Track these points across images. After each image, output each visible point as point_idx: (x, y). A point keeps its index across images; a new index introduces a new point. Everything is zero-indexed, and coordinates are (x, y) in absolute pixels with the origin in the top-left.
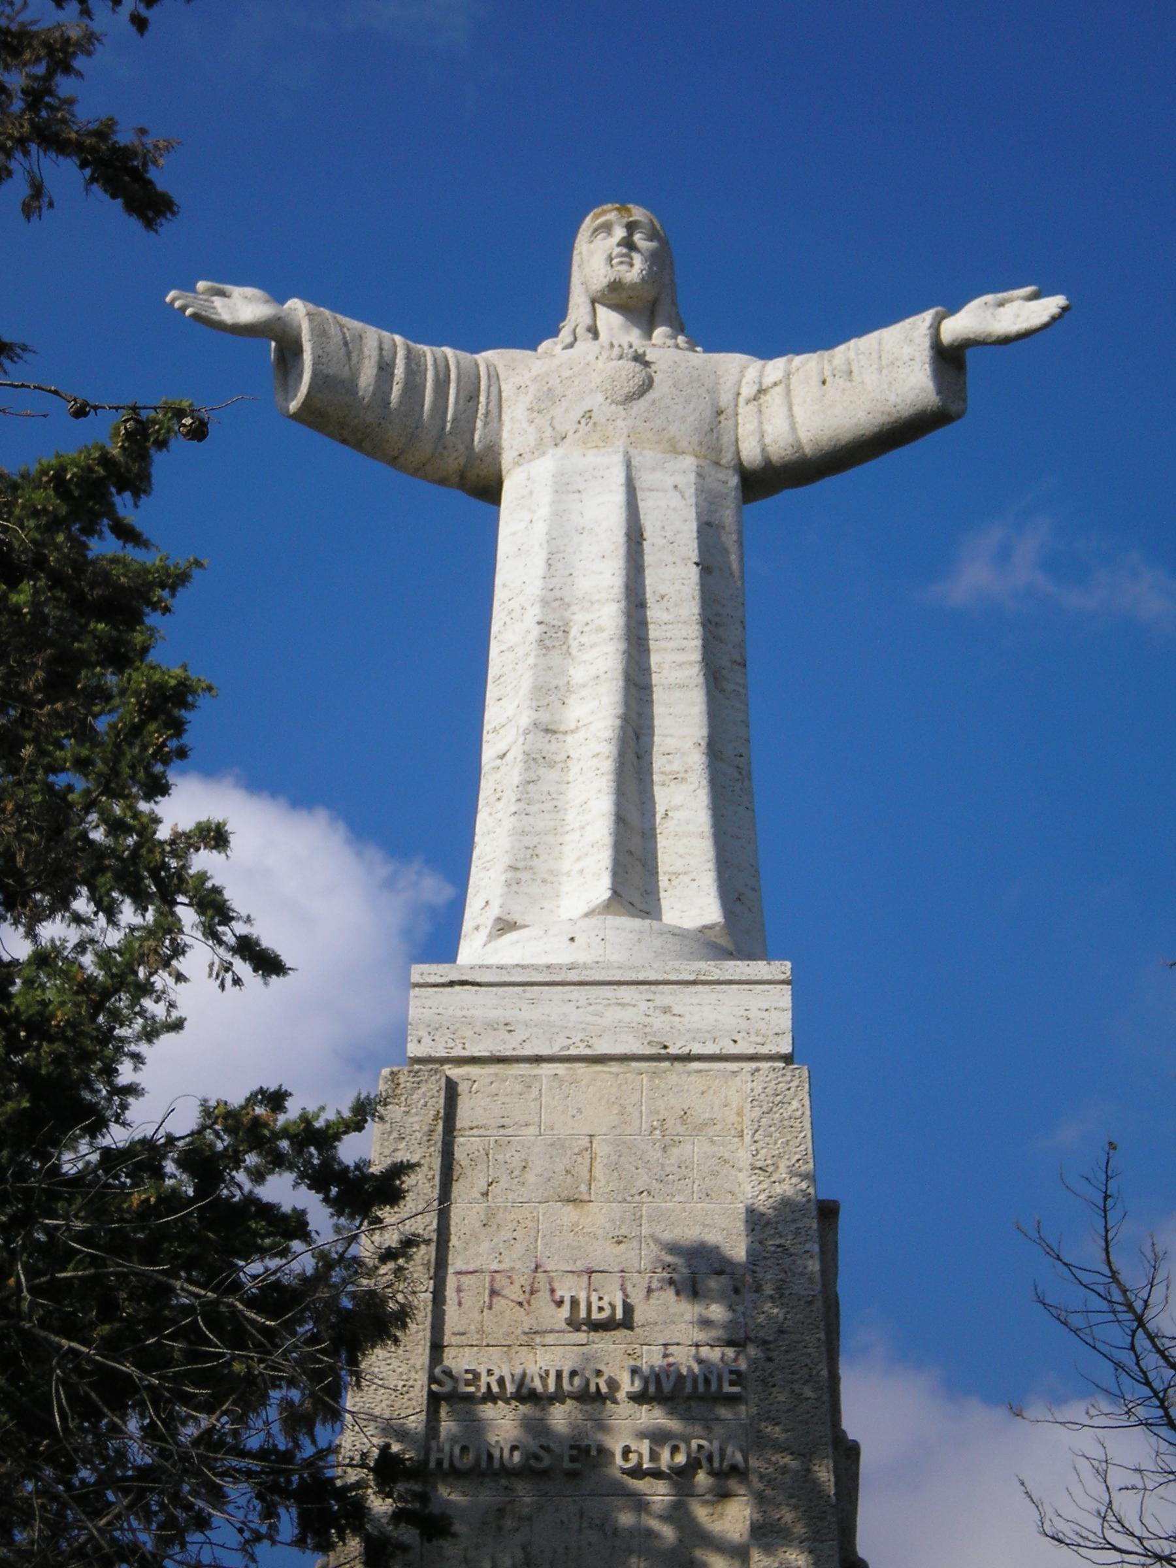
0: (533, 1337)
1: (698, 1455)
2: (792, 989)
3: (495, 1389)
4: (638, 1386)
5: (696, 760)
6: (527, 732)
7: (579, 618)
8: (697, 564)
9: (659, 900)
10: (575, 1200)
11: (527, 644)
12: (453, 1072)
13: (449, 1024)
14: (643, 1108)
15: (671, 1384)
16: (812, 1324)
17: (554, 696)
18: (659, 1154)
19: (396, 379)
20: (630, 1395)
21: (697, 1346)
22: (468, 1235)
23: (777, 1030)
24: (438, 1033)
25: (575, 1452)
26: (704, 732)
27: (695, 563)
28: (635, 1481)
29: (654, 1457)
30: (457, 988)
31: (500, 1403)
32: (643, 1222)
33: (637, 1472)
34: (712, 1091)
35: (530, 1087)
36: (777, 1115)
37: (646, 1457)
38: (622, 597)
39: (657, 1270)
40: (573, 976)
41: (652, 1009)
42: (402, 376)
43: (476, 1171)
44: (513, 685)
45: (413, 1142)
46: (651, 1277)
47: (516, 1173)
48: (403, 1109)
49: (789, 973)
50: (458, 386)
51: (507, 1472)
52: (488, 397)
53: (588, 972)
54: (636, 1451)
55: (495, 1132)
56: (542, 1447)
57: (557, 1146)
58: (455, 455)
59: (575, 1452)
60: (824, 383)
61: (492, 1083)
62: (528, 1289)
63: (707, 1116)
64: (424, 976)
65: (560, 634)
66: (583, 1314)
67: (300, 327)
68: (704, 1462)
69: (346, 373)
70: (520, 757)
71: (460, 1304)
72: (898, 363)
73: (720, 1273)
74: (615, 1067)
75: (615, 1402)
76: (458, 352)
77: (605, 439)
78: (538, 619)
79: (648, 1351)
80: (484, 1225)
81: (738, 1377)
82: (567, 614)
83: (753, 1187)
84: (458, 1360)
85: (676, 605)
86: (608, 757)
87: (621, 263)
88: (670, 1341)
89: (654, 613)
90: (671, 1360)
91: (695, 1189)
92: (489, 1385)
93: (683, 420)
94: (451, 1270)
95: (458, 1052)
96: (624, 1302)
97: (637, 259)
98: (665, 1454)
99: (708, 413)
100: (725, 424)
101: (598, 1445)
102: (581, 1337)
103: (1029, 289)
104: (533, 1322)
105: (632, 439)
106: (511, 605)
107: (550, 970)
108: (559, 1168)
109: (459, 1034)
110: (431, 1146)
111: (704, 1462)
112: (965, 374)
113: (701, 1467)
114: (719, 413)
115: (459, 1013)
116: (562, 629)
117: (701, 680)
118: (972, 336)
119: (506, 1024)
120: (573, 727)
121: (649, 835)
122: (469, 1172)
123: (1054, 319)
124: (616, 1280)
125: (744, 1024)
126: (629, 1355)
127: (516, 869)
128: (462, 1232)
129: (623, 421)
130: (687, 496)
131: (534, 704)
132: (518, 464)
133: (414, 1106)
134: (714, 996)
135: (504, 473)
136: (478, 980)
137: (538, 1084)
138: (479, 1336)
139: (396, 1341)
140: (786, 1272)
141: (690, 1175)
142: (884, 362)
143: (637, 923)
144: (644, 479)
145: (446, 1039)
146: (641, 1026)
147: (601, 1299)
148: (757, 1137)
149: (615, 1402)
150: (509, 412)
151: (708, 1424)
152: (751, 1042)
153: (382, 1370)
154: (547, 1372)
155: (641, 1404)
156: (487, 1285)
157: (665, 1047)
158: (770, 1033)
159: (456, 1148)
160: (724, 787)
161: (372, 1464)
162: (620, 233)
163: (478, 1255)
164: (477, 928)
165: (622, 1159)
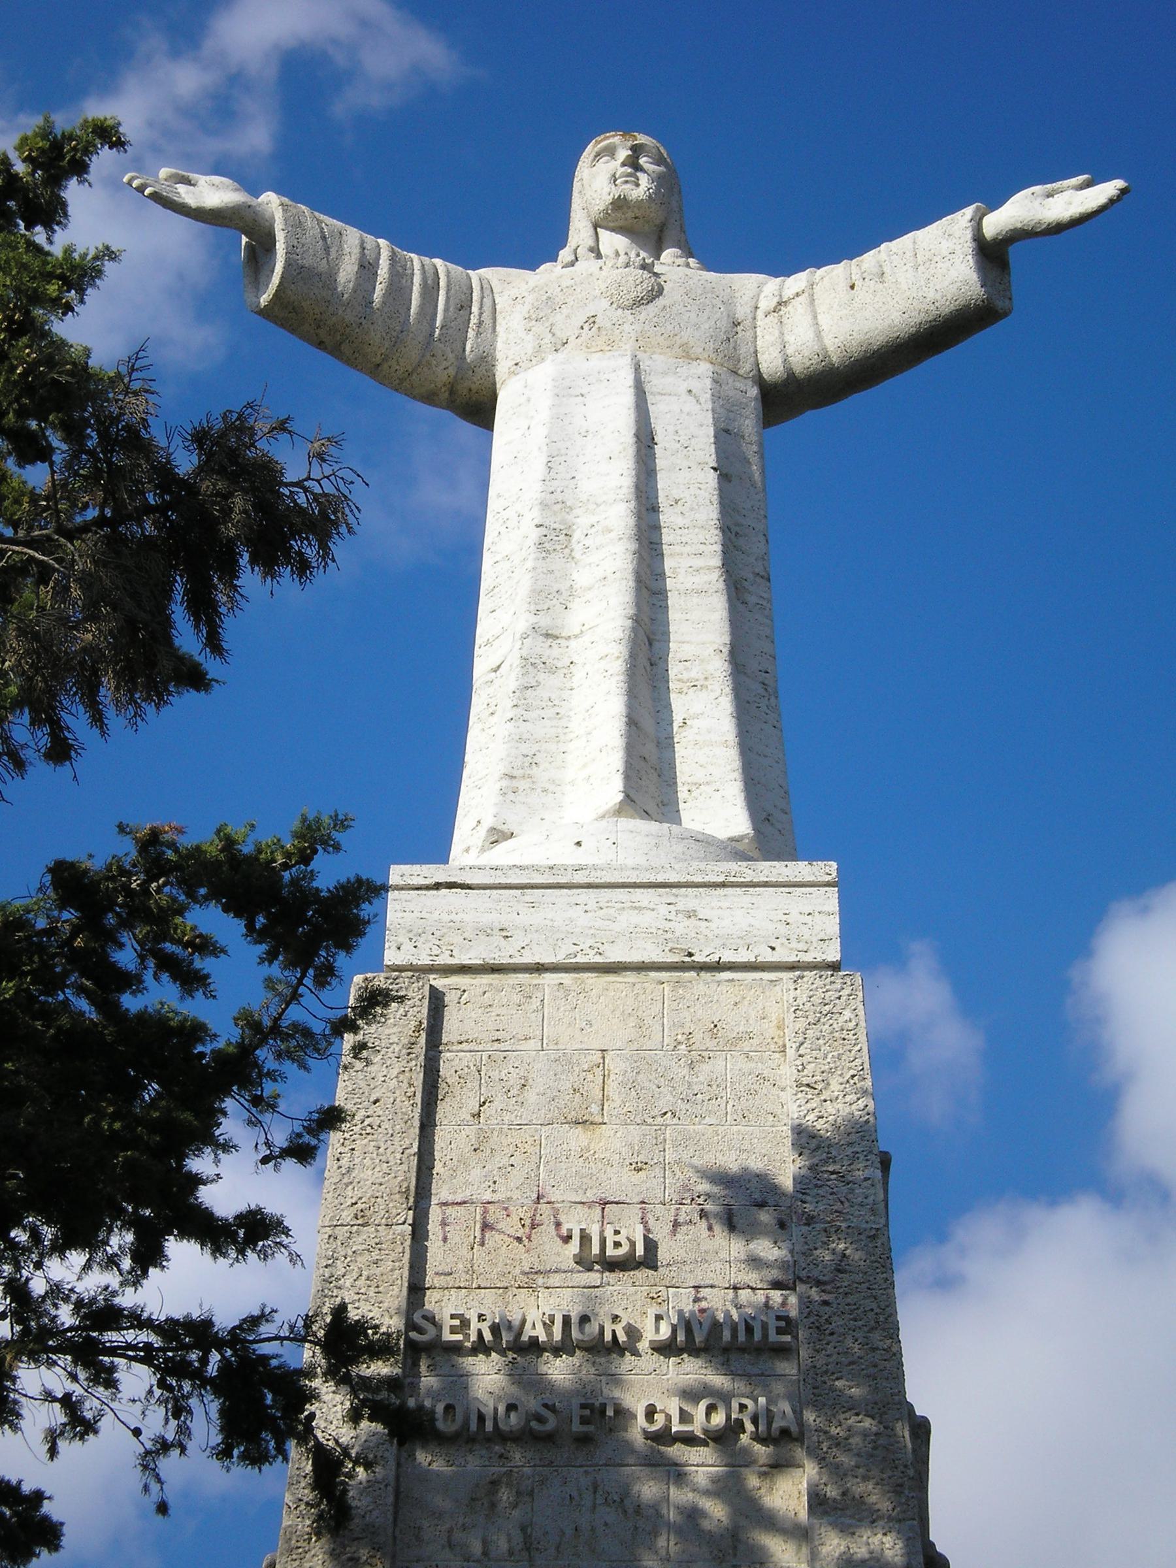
0: (533, 1280)
3: (488, 1336)
4: (665, 1332)
5: (718, 668)
6: (525, 636)
7: (582, 521)
8: (715, 469)
9: (678, 811)
10: (585, 1122)
11: (524, 549)
12: (439, 982)
13: (434, 930)
14: (665, 1020)
17: (555, 600)
18: (685, 1071)
19: (379, 279)
20: (655, 1345)
21: (735, 1288)
24: (422, 939)
25: (587, 1412)
26: (727, 639)
27: (712, 468)
29: (685, 1417)
30: (444, 891)
31: (493, 1354)
32: (667, 1147)
33: (664, 1437)
34: (746, 1002)
35: (531, 997)
36: (827, 1026)
37: (675, 1419)
38: (632, 497)
39: (684, 1201)
40: (580, 878)
41: (674, 913)
42: (386, 276)
43: (465, 1089)
44: (509, 593)
45: (390, 1055)
46: (678, 1209)
47: (514, 1092)
49: (834, 874)
51: (500, 1436)
53: (599, 874)
54: (662, 1411)
55: (489, 1046)
56: (546, 1406)
57: (563, 1061)
58: (445, 364)
59: (587, 1412)
60: (852, 287)
61: (485, 993)
62: (528, 1222)
63: (741, 1029)
64: (405, 878)
65: (562, 537)
66: (596, 1250)
67: (273, 218)
68: (749, 1427)
69: (323, 266)
70: (517, 662)
71: (445, 1240)
72: (936, 259)
74: (631, 977)
75: (636, 1353)
76: (451, 266)
77: (611, 344)
78: (537, 522)
79: (675, 1295)
80: (475, 1150)
81: (787, 1324)
82: (570, 518)
83: (800, 1106)
84: (443, 1304)
85: (692, 509)
86: (618, 658)
87: (627, 182)
88: (702, 1283)
89: (667, 517)
90: (704, 1304)
91: (728, 1110)
92: (480, 1333)
93: (697, 327)
94: (434, 1201)
95: (444, 959)
97: (644, 179)
99: (724, 324)
100: (743, 335)
101: (615, 1404)
102: (594, 1278)
105: (641, 343)
106: (505, 514)
107: (554, 871)
111: (749, 1427)
112: (1009, 274)
113: (744, 1432)
114: (736, 324)
115: (446, 918)
116: (564, 532)
117: (721, 585)
118: (1019, 225)
119: (502, 930)
120: (576, 632)
121: (666, 744)
122: (457, 1090)
123: (1112, 202)
124: (635, 1211)
125: (783, 930)
127: (513, 777)
128: (449, 1157)
129: (631, 325)
130: (702, 400)
131: (533, 608)
132: (514, 373)
133: (391, 1016)
135: (498, 386)
136: (468, 882)
137: (539, 995)
138: (468, 1277)
139: (303, 568)
140: (842, 1202)
141: (723, 1094)
142: (920, 258)
143: (653, 827)
144: (654, 384)
146: (661, 932)
147: (617, 1232)
149: (636, 1353)
150: (504, 323)
152: (792, 949)
154: (552, 1319)
155: (667, 1356)
156: (478, 1217)
157: (690, 955)
158: (814, 939)
160: (748, 702)
161: (321, 1334)
162: (623, 154)
163: (467, 1183)
164: (467, 850)
165: (641, 1076)
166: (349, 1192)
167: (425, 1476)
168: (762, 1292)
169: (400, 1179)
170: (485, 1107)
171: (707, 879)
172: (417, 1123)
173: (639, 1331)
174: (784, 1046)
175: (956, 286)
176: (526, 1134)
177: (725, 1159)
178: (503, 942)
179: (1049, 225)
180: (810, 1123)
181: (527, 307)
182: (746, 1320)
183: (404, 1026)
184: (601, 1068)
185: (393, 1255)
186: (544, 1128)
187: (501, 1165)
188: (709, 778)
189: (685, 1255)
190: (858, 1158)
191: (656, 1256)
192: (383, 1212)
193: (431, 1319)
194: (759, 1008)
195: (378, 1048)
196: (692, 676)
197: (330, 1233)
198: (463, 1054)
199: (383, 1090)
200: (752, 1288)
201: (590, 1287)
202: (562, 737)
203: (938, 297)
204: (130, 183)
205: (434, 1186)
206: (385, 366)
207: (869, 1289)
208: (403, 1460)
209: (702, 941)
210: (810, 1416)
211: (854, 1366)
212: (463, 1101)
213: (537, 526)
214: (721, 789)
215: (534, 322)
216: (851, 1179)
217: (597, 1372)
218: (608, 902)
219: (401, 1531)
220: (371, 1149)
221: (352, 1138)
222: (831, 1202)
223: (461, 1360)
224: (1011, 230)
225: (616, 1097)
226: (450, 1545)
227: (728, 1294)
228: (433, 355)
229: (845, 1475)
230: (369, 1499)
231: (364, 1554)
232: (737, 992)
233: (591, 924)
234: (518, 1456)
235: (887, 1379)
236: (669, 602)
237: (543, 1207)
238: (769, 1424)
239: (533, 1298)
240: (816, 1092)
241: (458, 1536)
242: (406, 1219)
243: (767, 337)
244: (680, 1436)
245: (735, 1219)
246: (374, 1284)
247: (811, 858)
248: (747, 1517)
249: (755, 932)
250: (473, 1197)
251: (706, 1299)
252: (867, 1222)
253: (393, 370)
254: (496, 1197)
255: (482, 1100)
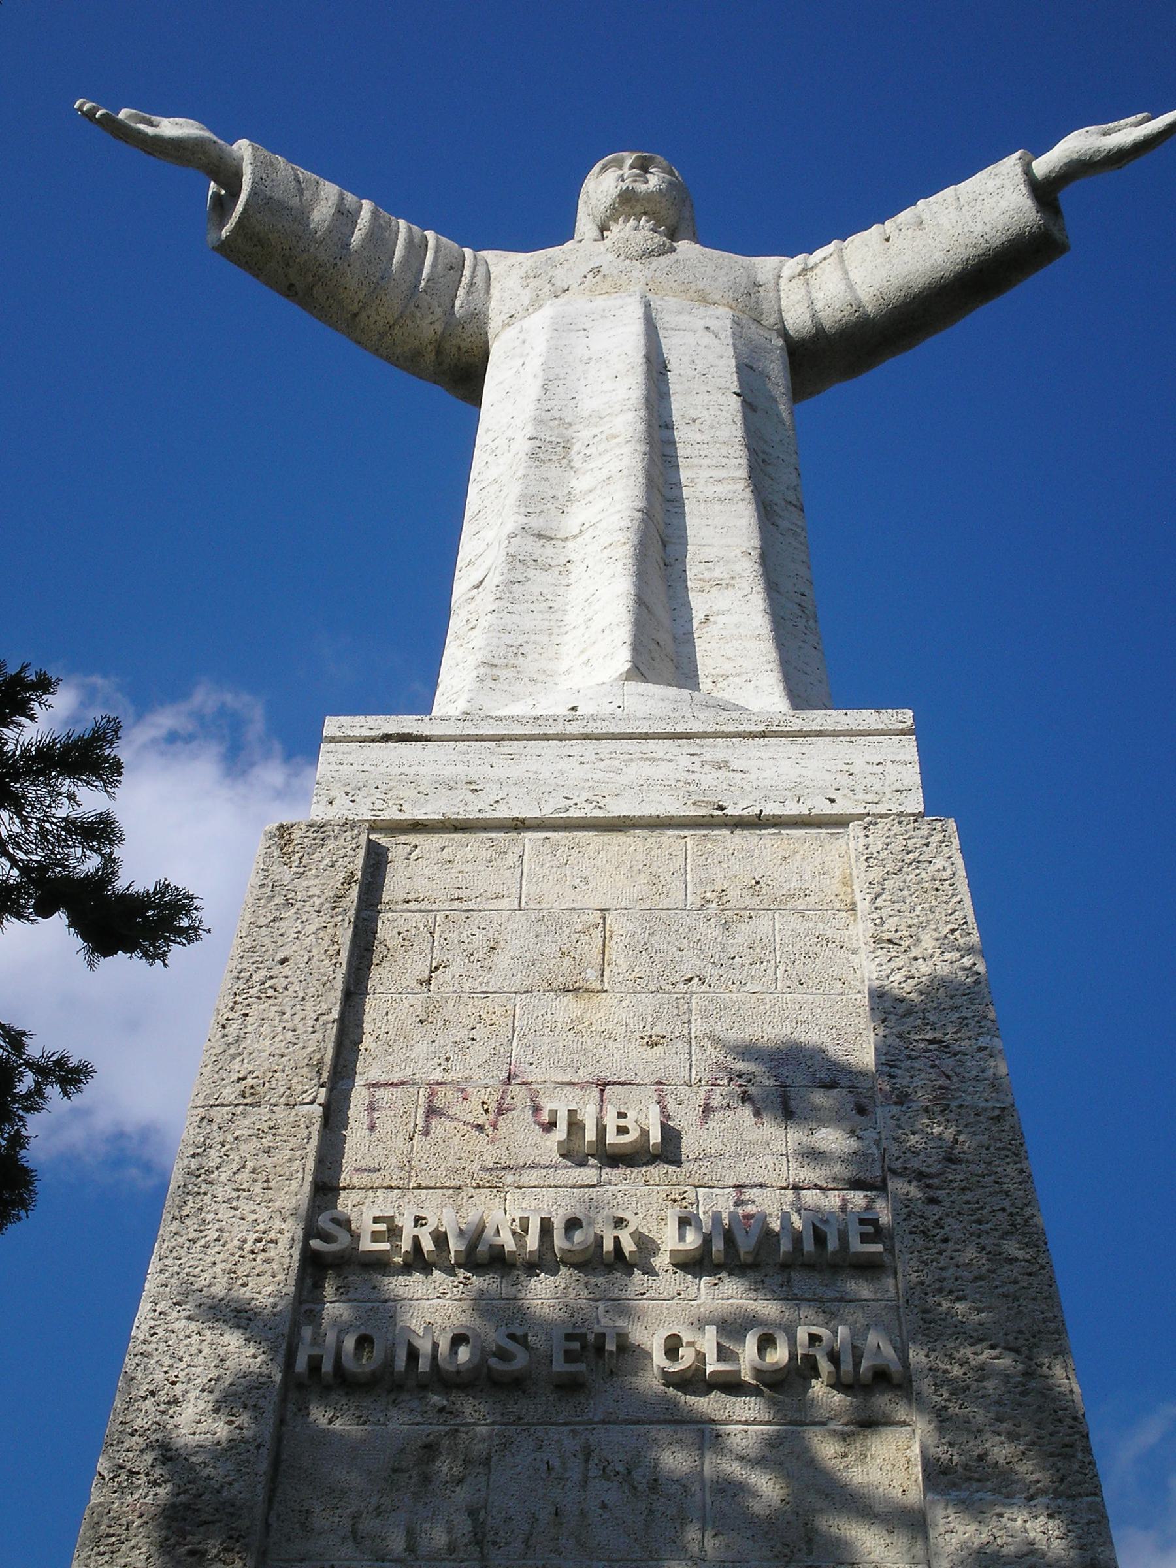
1: (812, 1352)
2: (919, 731)
3: (428, 1245)
4: (692, 1240)
5: (748, 570)
8: (738, 395)
10: (577, 990)
14: (688, 877)
15: (753, 1241)
16: (1004, 1148)
18: (717, 932)
20: (680, 1259)
22: (392, 1035)
23: (898, 786)
24: (363, 793)
25: (576, 1345)
26: (757, 543)
27: (734, 393)
28: (691, 1399)
31: (436, 1273)
32: (693, 1018)
35: (505, 853)
36: (912, 876)
39: (718, 1082)
45: (307, 909)
48: (294, 869)
49: (910, 722)
50: (436, 252)
52: (474, 272)
53: (599, 724)
54: (691, 1344)
55: (446, 906)
56: (512, 1337)
60: (887, 240)
62: (493, 1106)
66: (591, 1135)
68: (824, 1366)
71: (372, 1128)
73: (830, 1086)
75: (650, 1271)
80: (421, 1022)
83: (880, 965)
85: (712, 427)
88: (748, 1182)
90: (750, 1209)
91: (778, 976)
92: (416, 1241)
94: (359, 1081)
96: (663, 1126)
98: (748, 1351)
101: (618, 1335)
102: (588, 1174)
103: (1140, 116)
104: (503, 1153)
108: (551, 947)
109: (394, 793)
110: (337, 914)
111: (824, 1366)
113: (817, 1375)
115: (395, 770)
116: (562, 444)
117: (748, 494)
118: (1075, 156)
120: (576, 531)
122: (399, 954)
126: (675, 1201)
130: (722, 336)
131: (522, 510)
134: (797, 748)
137: (518, 850)
140: (948, 1077)
142: (962, 202)
144: (666, 320)
145: (373, 799)
148: (879, 903)
149: (650, 1271)
151: (830, 1309)
152: (857, 801)
153: (220, 1216)
154: (525, 1221)
156: (422, 1100)
157: (721, 808)
159: (380, 923)
163: (408, 1061)
165: (656, 937)
166: (236, 1064)
167: (324, 1438)
168: (836, 1193)
169: (310, 1049)
170: (438, 972)
171: (741, 728)
172: (339, 985)
173: (654, 1242)
174: (854, 904)
175: (1007, 216)
176: (494, 1003)
177: (776, 1031)
178: (470, 796)
179: (1109, 152)
180: (895, 984)
181: (524, 269)
182: (814, 1225)
183: (329, 878)
184: (600, 929)
185: (293, 1142)
186: (519, 997)
187: (457, 1039)
188: (738, 670)
189: (721, 1146)
190: (967, 1025)
191: (679, 1148)
192: (282, 1090)
193: (345, 1223)
194: (816, 863)
195: (291, 901)
196: (716, 575)
197: (203, 1115)
198: (410, 914)
199: (294, 948)
200: (821, 1189)
201: (581, 1187)
202: (556, 630)
203: (987, 229)
204: (80, 109)
205: (360, 1063)
206: (363, 316)
207: (997, 1183)
208: (289, 1415)
209: (737, 793)
210: (917, 1356)
211: (982, 1283)
212: (408, 966)
213: (530, 439)
214: (754, 679)
215: (532, 279)
216: (958, 1049)
217: (591, 1296)
218: (611, 753)
219: (278, 1516)
220: (272, 1014)
221: (246, 1002)
222: (933, 1077)
223: (386, 1280)
224: (1065, 164)
225: (620, 961)
226: (356, 1537)
227: (785, 1195)
228: (418, 307)
229: (980, 1431)
230: (230, 1466)
231: (213, 1547)
232: (785, 847)
233: (589, 776)
234: (468, 1410)
235: (1034, 1299)
236: (686, 508)
237: (515, 1089)
238: (857, 1364)
239: (497, 1200)
240: (902, 948)
241: (368, 1524)
242: (316, 1097)
243: (792, 297)
244: (721, 1380)
245: (793, 1104)
246: (262, 1177)
247: (877, 704)
248: (827, 1496)
249: (807, 783)
250: (417, 1076)
251: (754, 1202)
252: (986, 1100)
253: (372, 320)
254: (448, 1077)
255: (434, 965)
